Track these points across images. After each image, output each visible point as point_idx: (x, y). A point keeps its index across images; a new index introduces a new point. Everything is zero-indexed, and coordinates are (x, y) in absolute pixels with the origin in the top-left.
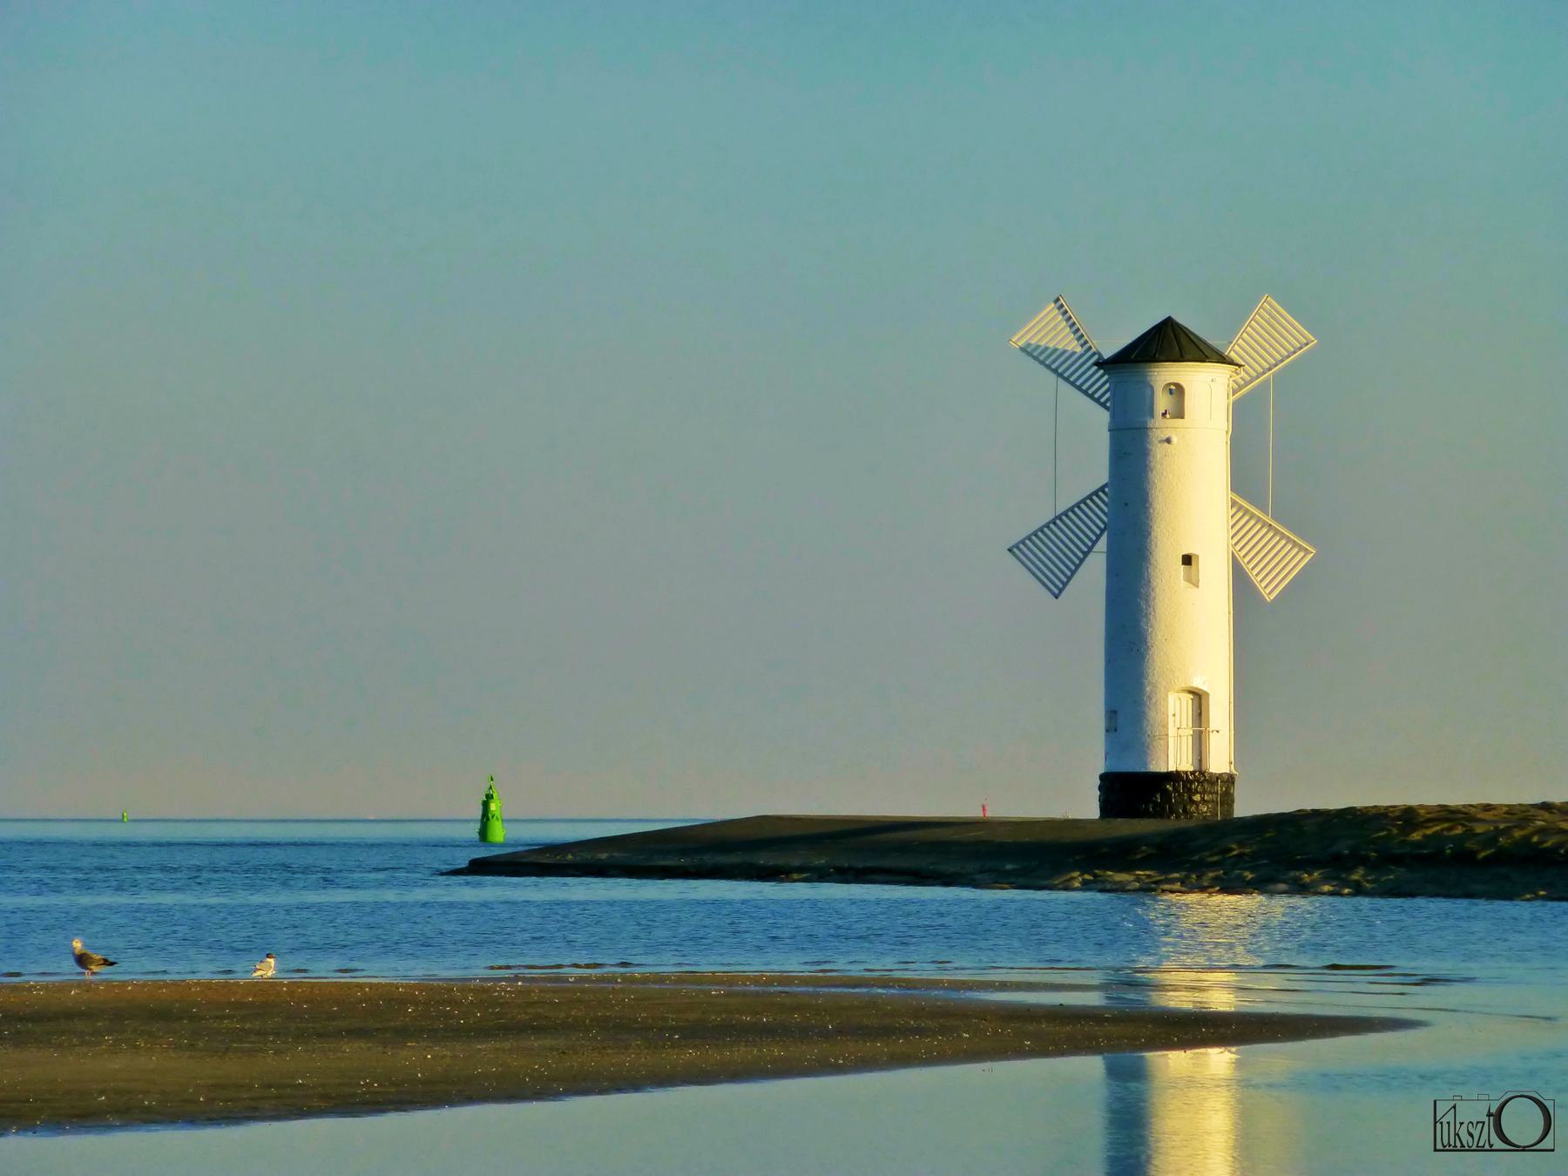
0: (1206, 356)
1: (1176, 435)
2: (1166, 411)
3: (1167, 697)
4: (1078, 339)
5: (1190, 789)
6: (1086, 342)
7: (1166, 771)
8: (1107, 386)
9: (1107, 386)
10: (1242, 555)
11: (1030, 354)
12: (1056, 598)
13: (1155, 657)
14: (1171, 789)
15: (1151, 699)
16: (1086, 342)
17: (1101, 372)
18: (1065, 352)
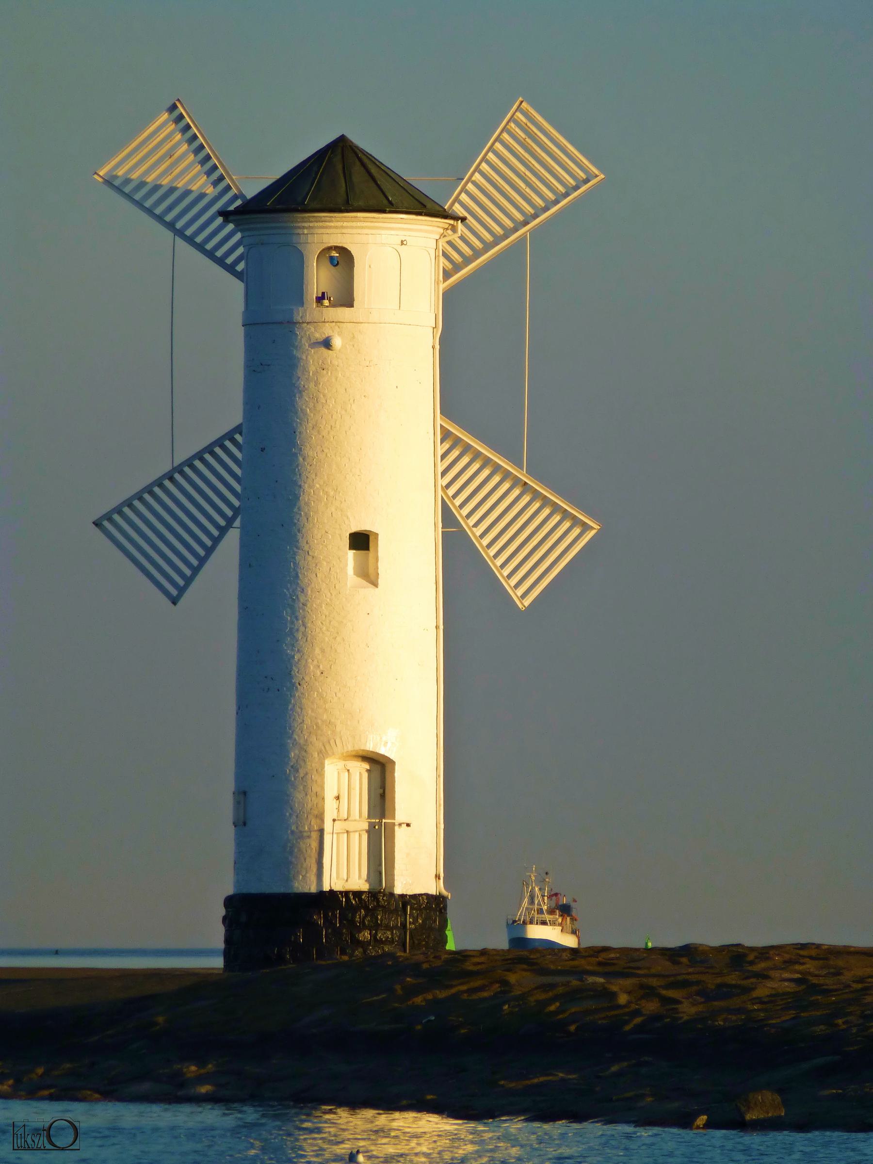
0: (390, 203)
1: (340, 334)
2: (323, 294)
3: (323, 767)
4: (209, 173)
5: (352, 922)
6: (221, 178)
7: (313, 889)
8: (240, 250)
9: (240, 250)
10: (478, 534)
11: (118, 190)
12: (174, 603)
13: (304, 701)
14: (321, 922)
15: (297, 771)
16: (221, 178)
17: (231, 226)
18: (188, 192)
